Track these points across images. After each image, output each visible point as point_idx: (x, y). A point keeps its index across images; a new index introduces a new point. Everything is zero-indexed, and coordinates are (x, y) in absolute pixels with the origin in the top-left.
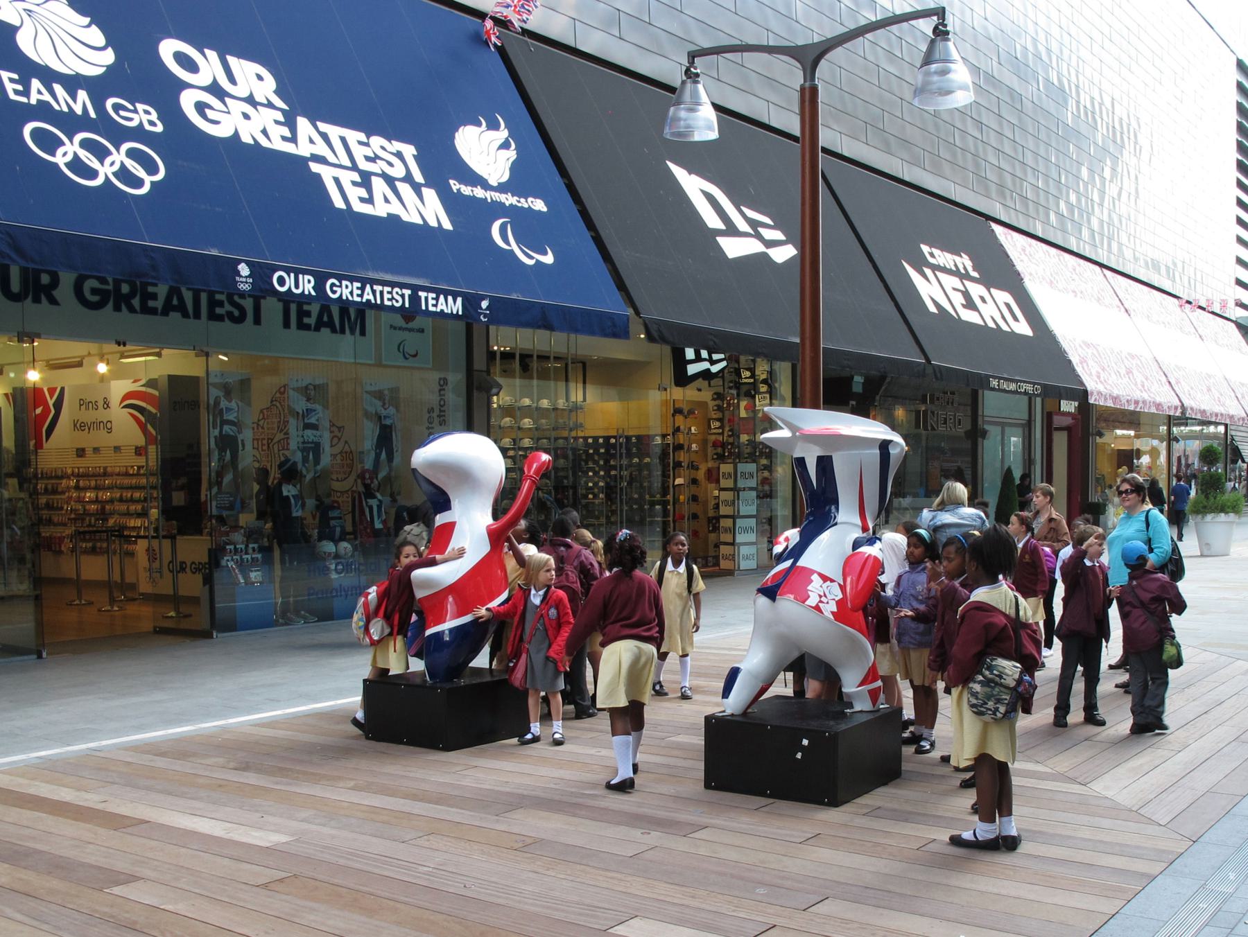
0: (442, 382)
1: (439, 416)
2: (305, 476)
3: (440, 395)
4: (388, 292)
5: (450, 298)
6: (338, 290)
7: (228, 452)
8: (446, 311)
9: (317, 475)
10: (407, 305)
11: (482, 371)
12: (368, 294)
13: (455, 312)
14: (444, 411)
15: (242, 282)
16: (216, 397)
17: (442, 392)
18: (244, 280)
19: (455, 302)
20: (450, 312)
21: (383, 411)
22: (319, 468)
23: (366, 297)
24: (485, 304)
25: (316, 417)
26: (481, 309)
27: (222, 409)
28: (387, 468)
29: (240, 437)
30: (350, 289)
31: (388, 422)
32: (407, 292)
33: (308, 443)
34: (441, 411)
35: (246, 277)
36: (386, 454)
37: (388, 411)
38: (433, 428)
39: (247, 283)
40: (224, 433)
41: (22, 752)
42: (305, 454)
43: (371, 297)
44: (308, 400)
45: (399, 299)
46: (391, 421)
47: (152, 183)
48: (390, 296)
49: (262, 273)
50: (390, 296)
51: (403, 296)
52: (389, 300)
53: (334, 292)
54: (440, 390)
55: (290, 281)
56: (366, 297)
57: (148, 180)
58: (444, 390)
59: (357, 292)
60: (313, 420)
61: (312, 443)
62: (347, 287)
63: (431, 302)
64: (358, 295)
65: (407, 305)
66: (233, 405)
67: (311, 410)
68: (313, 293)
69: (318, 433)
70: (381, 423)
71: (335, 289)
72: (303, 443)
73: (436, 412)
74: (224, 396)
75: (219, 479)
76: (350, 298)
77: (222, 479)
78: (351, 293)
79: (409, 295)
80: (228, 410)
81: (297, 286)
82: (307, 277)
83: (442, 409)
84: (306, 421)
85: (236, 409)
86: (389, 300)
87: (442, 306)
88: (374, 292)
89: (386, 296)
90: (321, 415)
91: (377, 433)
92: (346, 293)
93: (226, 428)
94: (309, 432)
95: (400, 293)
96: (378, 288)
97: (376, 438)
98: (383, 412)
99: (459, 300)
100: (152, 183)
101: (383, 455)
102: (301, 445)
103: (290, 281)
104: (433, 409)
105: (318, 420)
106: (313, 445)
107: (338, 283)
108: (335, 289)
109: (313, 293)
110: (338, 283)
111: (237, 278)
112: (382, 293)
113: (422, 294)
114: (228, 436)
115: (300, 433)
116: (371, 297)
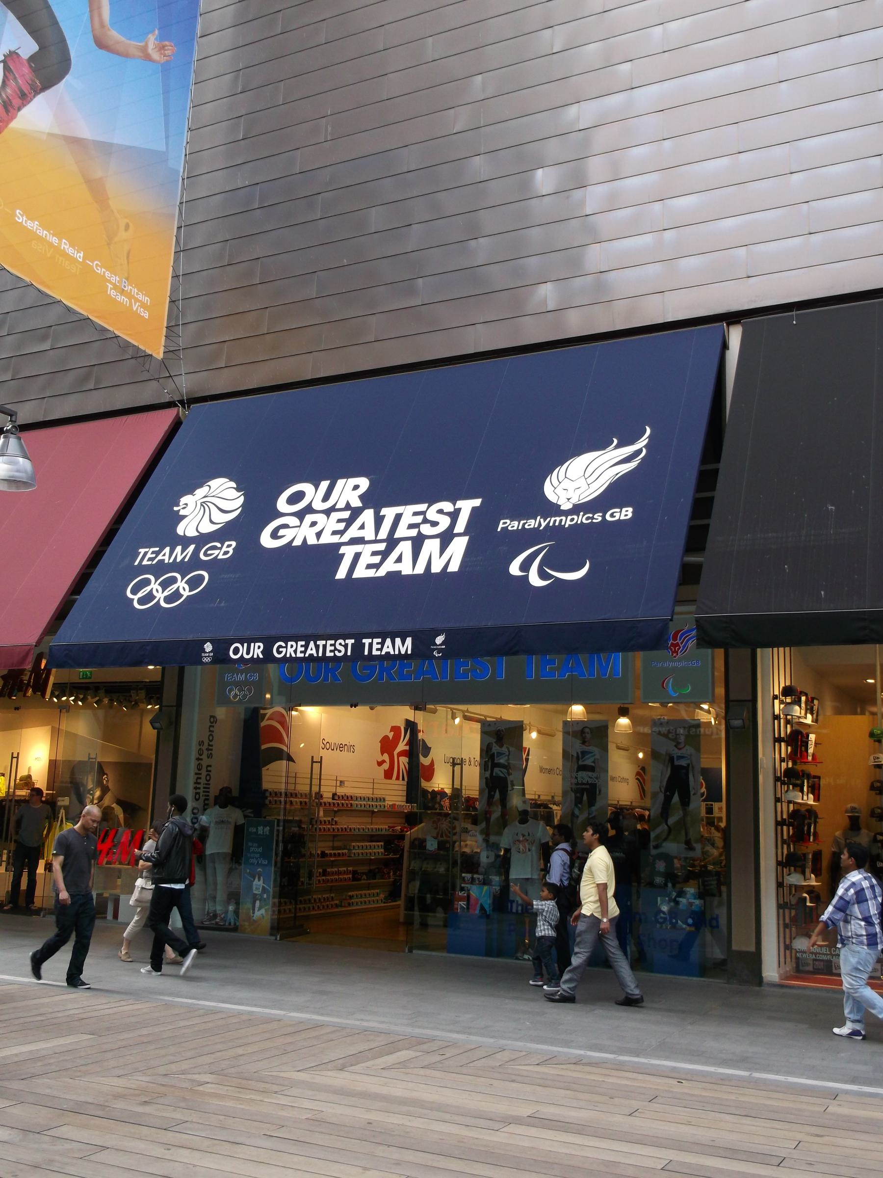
0: (212, 720)
1: (208, 750)
2: (578, 817)
3: (210, 731)
4: (331, 645)
5: (398, 641)
6: (284, 650)
7: (497, 791)
8: (392, 653)
9: (591, 816)
10: (349, 653)
11: (172, 706)
12: (312, 649)
13: (403, 652)
14: (212, 746)
15: (205, 657)
16: (489, 744)
17: (211, 729)
18: (207, 655)
19: (403, 643)
20: (397, 652)
21: (676, 751)
22: (594, 808)
23: (309, 652)
24: (439, 640)
25: (592, 759)
26: (436, 645)
27: (494, 753)
28: (681, 812)
29: (510, 778)
30: (294, 648)
31: (683, 763)
32: (350, 642)
33: (583, 784)
34: (209, 745)
35: (209, 652)
36: (680, 796)
37: (683, 751)
38: (201, 759)
39: (209, 656)
40: (494, 774)
41: (703, 1064)
42: (578, 795)
43: (314, 652)
44: (584, 742)
45: (343, 649)
46: (688, 762)
47: (133, 600)
48: (333, 648)
49: (221, 647)
50: (333, 648)
51: (346, 646)
52: (331, 651)
53: (279, 652)
54: (210, 726)
55: (243, 651)
56: (309, 652)
57: (136, 598)
58: (213, 726)
59: (300, 649)
60: (589, 762)
61: (587, 784)
62: (292, 646)
63: (375, 646)
64: (301, 652)
65: (349, 653)
66: (504, 749)
67: (586, 752)
68: (261, 656)
69: (595, 775)
70: (578, 764)
71: (281, 650)
72: (577, 784)
73: (206, 746)
74: (495, 742)
75: (488, 816)
76: (294, 655)
77: (490, 816)
78: (295, 651)
79: (352, 644)
80: (500, 754)
81: (248, 653)
82: (257, 644)
83: (211, 743)
84: (581, 763)
85: (507, 754)
86: (331, 651)
87: (388, 648)
88: (317, 647)
89: (329, 648)
90: (597, 757)
91: (667, 776)
92: (290, 651)
93: (496, 770)
94: (582, 774)
95: (343, 644)
96: (321, 643)
97: (666, 779)
98: (676, 752)
99: (409, 641)
100: (133, 600)
101: (676, 798)
102: (574, 786)
103: (243, 651)
104: (203, 742)
105: (594, 762)
106: (588, 787)
107: (283, 645)
108: (281, 650)
109: (261, 656)
110: (283, 645)
111: (203, 655)
112: (325, 647)
113: (367, 641)
114: (498, 778)
115: (574, 774)
116: (314, 652)
